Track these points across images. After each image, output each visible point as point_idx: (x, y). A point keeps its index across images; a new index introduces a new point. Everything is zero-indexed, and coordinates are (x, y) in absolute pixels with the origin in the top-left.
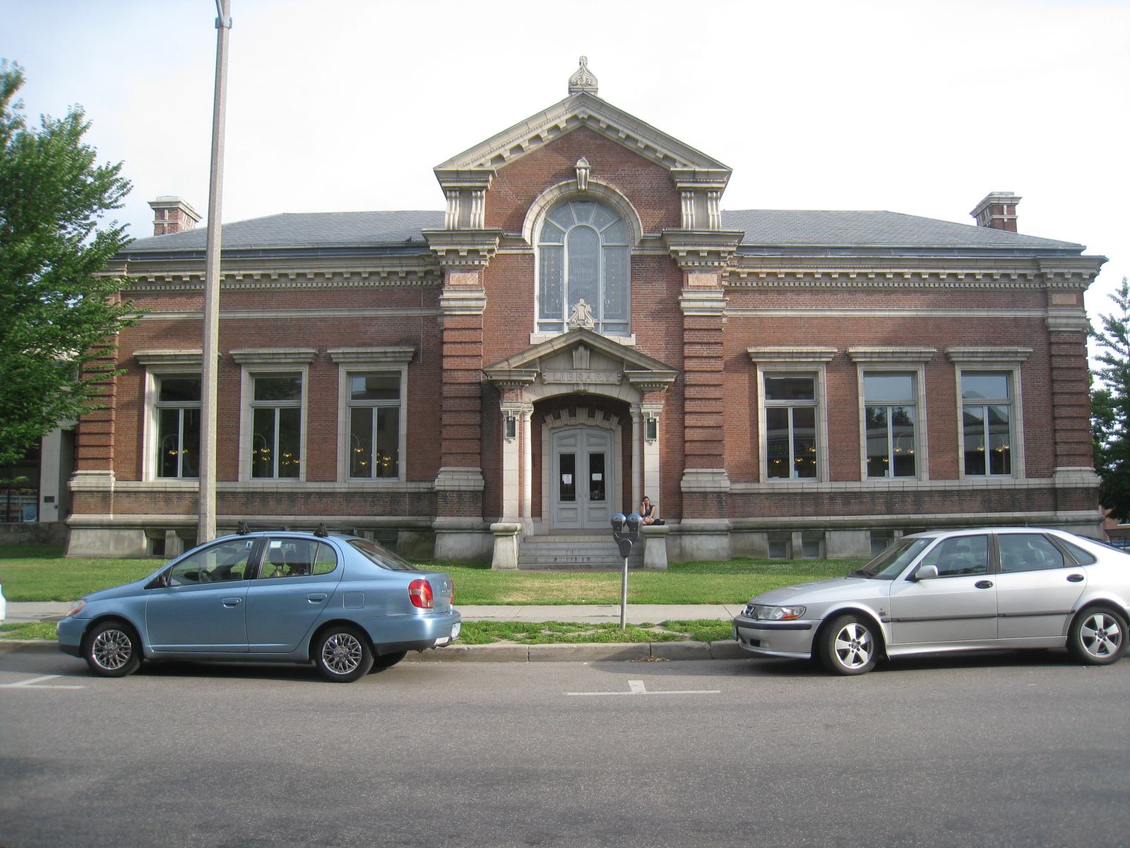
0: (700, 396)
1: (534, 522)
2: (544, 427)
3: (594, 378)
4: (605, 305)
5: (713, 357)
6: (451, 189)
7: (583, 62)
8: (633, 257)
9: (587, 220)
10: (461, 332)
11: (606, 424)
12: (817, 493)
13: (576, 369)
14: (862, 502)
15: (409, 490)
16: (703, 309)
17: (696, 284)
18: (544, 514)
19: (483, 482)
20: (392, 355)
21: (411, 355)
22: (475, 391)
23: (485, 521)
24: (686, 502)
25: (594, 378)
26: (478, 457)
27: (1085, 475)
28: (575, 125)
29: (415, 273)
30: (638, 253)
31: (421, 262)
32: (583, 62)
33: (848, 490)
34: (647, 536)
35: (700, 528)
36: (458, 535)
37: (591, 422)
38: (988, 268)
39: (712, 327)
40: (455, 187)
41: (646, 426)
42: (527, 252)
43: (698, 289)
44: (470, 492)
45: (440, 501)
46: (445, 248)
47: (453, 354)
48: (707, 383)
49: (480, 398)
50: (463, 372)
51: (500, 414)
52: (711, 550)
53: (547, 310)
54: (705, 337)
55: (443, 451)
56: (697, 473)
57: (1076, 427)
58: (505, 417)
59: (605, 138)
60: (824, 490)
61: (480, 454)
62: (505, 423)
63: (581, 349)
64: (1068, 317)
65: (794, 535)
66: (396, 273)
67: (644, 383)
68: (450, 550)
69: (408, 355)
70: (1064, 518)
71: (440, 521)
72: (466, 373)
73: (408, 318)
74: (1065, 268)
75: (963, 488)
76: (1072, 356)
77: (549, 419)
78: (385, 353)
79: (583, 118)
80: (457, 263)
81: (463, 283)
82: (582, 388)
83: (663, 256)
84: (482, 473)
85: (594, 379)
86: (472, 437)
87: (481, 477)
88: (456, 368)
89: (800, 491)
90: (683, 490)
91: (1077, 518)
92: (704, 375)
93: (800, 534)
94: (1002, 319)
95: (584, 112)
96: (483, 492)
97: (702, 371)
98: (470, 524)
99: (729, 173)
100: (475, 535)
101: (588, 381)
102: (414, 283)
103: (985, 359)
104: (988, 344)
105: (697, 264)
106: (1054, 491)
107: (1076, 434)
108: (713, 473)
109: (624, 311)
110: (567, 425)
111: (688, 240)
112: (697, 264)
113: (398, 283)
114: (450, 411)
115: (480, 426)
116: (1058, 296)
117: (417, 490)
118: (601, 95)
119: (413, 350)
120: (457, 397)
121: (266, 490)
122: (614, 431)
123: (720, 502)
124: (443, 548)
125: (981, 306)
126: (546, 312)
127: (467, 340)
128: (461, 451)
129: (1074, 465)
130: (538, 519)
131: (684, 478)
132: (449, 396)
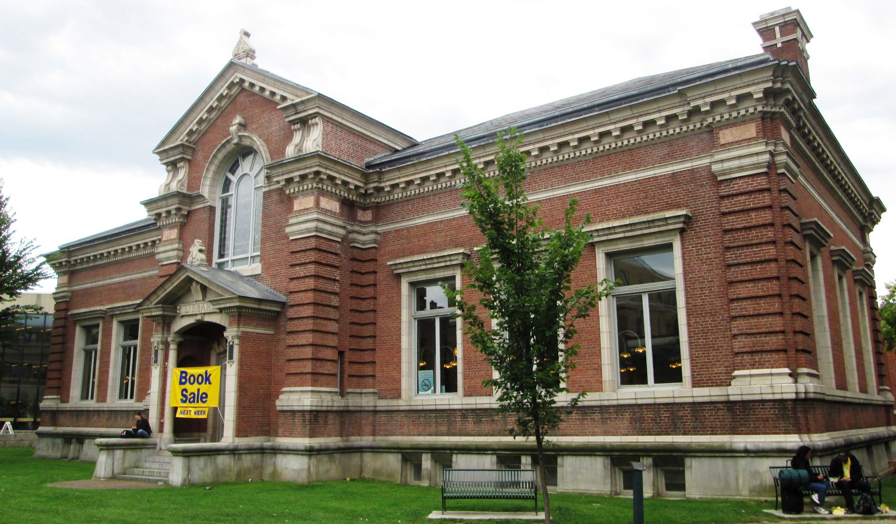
12: (450, 410)
14: (493, 420)
16: (301, 232)
27: (777, 380)
28: (235, 90)
30: (267, 189)
33: (479, 406)
38: (624, 120)
52: (294, 470)
56: (771, 374)
57: (762, 311)
60: (455, 407)
64: (740, 157)
65: (424, 456)
70: (741, 446)
74: (723, 92)
75: (606, 403)
76: (753, 209)
82: (199, 317)
89: (433, 407)
91: (762, 446)
93: (429, 455)
94: (655, 178)
98: (728, 444)
103: (627, 234)
104: (638, 213)
106: (730, 405)
107: (763, 320)
111: (285, 169)
116: (727, 131)
121: (640, 402)
125: (629, 167)
129: (761, 365)
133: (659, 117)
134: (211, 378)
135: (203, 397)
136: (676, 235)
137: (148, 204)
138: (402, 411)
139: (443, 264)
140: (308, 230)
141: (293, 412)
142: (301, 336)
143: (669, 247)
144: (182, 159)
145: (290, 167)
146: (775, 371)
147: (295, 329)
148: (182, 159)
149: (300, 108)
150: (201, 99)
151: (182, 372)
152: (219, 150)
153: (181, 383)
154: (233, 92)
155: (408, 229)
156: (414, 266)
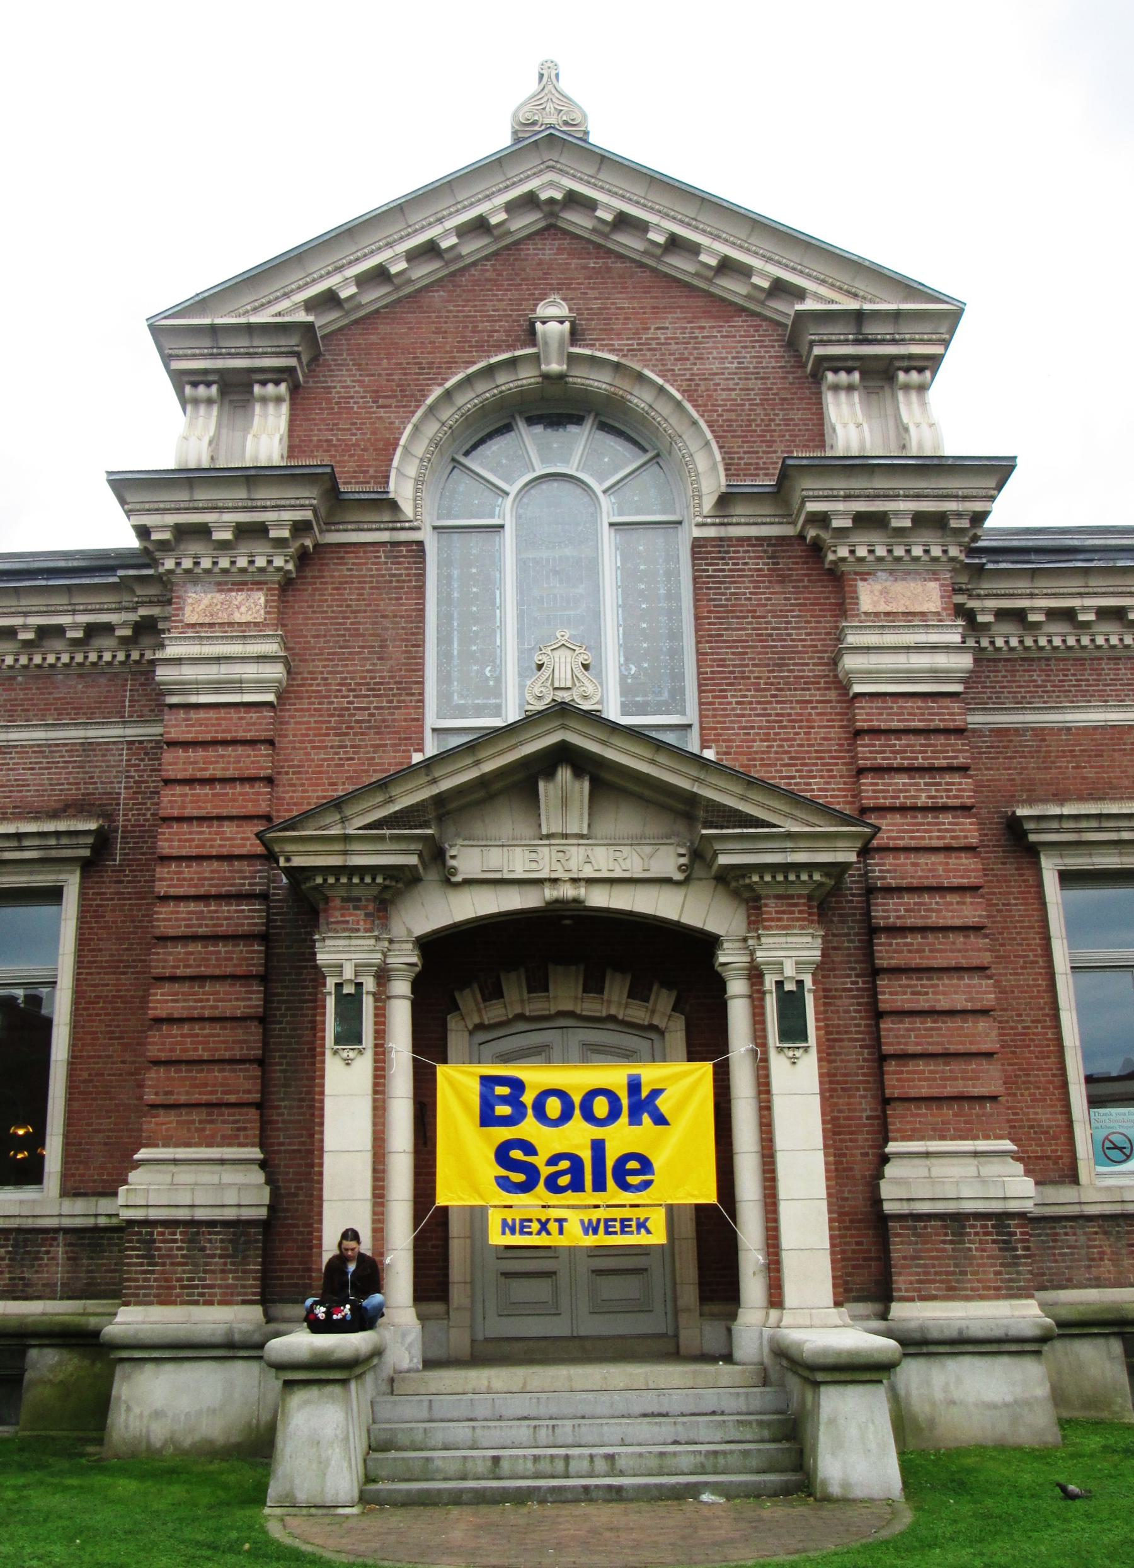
0: (920, 922)
1: (420, 1317)
2: (453, 1023)
3: (602, 861)
4: (623, 678)
5: (945, 808)
6: (198, 378)
7: (548, 75)
8: (698, 545)
9: (566, 461)
10: (211, 753)
11: (637, 1013)
13: (549, 836)
15: (67, 1223)
16: (910, 676)
17: (883, 608)
18: (458, 1294)
19: (267, 1189)
20: (37, 842)
21: (90, 840)
22: (246, 916)
23: (269, 1319)
24: (899, 1249)
25: (602, 861)
26: (253, 1114)
27: (993, 1168)
28: (527, 221)
29: (108, 628)
30: (711, 532)
31: (127, 599)
32: (548, 75)
34: (820, 1377)
35: (953, 1333)
36: (187, 1365)
37: (591, 1007)
39: (937, 723)
40: (206, 372)
41: (771, 1004)
42: (403, 536)
43: (889, 619)
44: (226, 1224)
45: (133, 1256)
46: (172, 519)
47: (187, 812)
48: (933, 882)
49: (264, 938)
50: (215, 865)
51: (318, 976)
52: (992, 1406)
53: (461, 696)
54: (919, 752)
55: (150, 1098)
56: (927, 1155)
58: (331, 982)
59: (609, 252)
61: (259, 1106)
62: (330, 1003)
63: (564, 774)
66: (59, 630)
67: (761, 868)
68: (157, 1414)
69: (82, 840)
71: (130, 1320)
72: (225, 866)
73: (88, 747)
77: (467, 1000)
78: (19, 836)
79: (551, 201)
80: (206, 563)
81: (223, 617)
82: (568, 892)
83: (782, 540)
84: (263, 1165)
85: (611, 866)
86: (238, 1054)
87: (259, 1177)
88: (194, 852)
90: (889, 1208)
92: (924, 860)
95: (551, 184)
96: (266, 1225)
97: (917, 850)
99: (954, 316)
100: (240, 1365)
101: (588, 872)
102: (107, 657)
105: (881, 551)
108: (976, 1154)
109: (678, 693)
110: (521, 1017)
111: (858, 484)
112: (881, 551)
113: (65, 658)
114: (173, 979)
115: (262, 1020)
117: (90, 1222)
118: (601, 137)
119: (93, 826)
120: (195, 938)
122: (661, 1033)
123: (1007, 1246)
124: (137, 1410)
126: (456, 699)
127: (229, 774)
128: (205, 1098)
130: (437, 1308)
131: (890, 1170)
132: (171, 932)
133: (1087, 605)
134: (663, 1104)
135: (634, 1170)
136: (72, 872)
137: (124, 486)
138: (1089, 1218)
139: (1113, 836)
140: (936, 675)
141: (956, 1221)
142: (945, 982)
143: (54, 895)
144: (278, 375)
145: (881, 483)
146: (982, 1145)
147: (917, 961)
148: (278, 375)
149: (871, 329)
150: (400, 210)
151: (488, 1082)
152: (468, 380)
153: (487, 1119)
154: (515, 226)
155: (1040, 733)
156: (1100, 830)
